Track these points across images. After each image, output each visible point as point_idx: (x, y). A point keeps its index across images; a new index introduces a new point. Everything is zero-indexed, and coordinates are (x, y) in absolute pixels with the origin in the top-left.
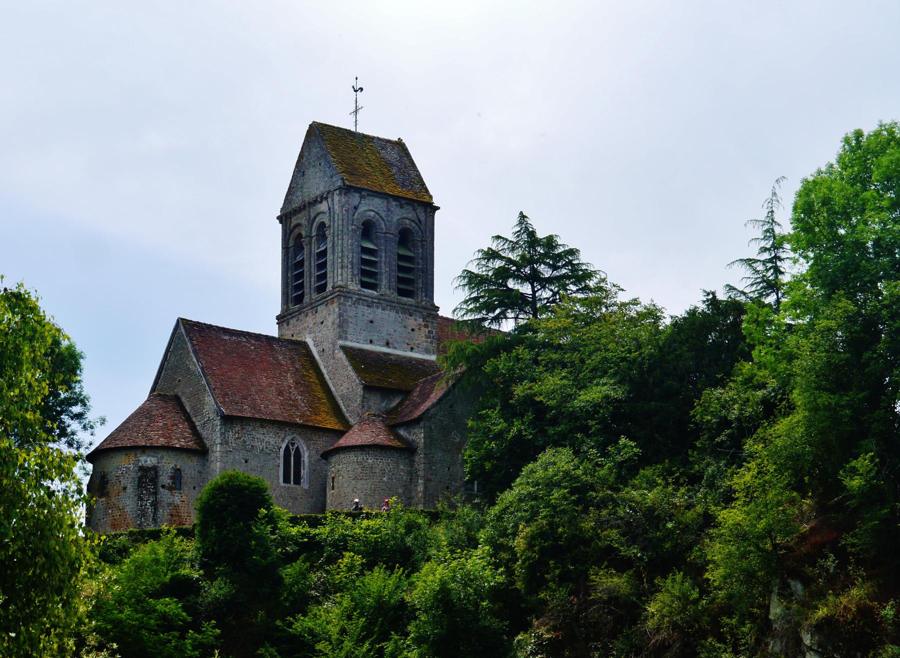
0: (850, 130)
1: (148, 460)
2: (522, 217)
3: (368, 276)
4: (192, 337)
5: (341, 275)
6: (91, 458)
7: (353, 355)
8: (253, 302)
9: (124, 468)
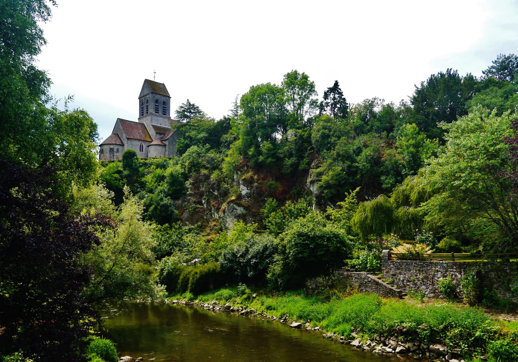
1: (112, 147)
3: (157, 111)
5: (151, 110)
6: (100, 146)
8: (133, 114)
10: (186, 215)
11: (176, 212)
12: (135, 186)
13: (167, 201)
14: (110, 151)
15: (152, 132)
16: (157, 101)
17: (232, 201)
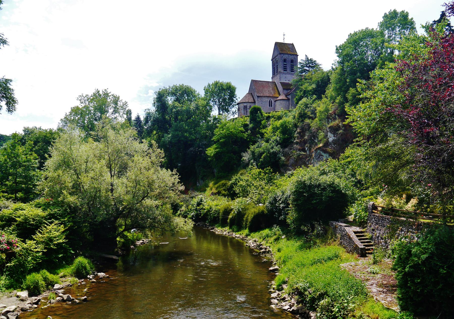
0: (349, 34)
1: (245, 104)
2: (306, 56)
3: (285, 69)
4: (254, 83)
5: (280, 69)
6: (238, 104)
7: (281, 83)
8: (266, 75)
9: (242, 105)
10: (291, 161)
11: (283, 158)
12: (257, 137)
13: (277, 149)
14: (244, 109)
15: (280, 88)
16: (285, 61)
17: (319, 148)
